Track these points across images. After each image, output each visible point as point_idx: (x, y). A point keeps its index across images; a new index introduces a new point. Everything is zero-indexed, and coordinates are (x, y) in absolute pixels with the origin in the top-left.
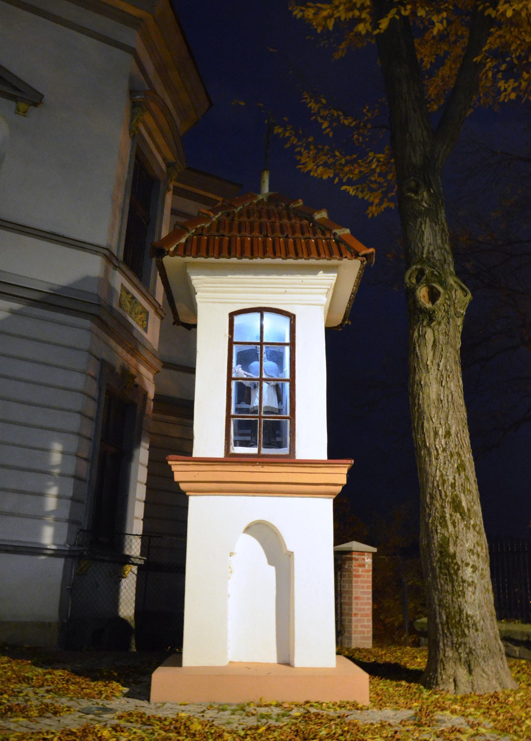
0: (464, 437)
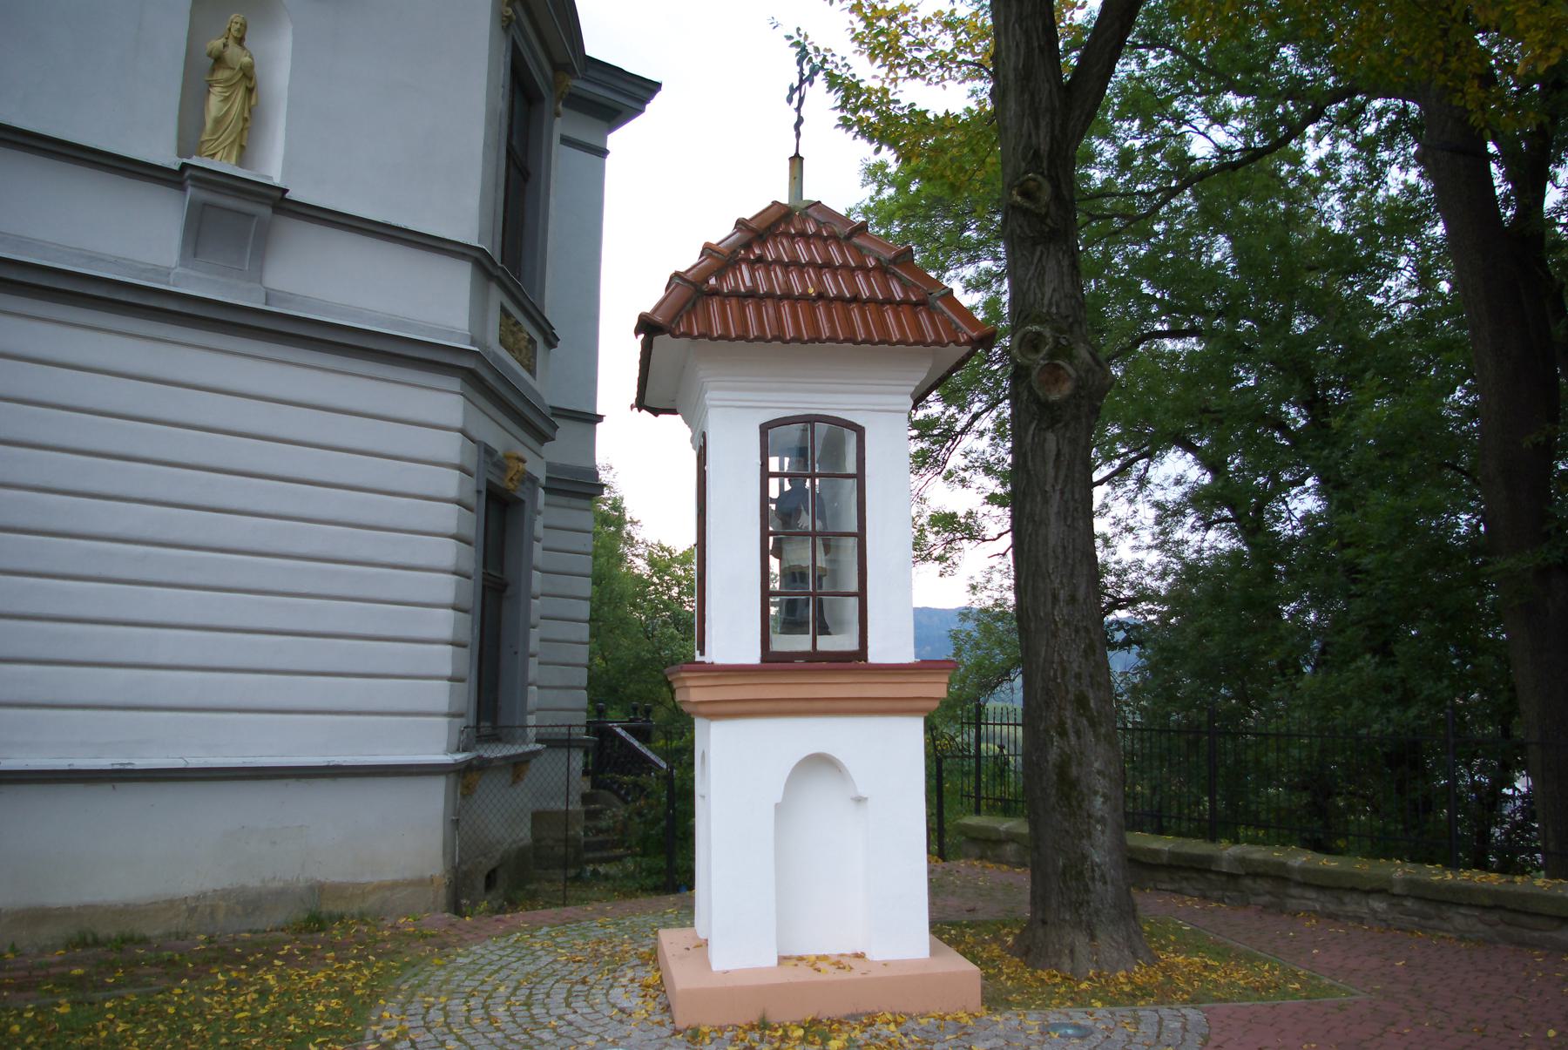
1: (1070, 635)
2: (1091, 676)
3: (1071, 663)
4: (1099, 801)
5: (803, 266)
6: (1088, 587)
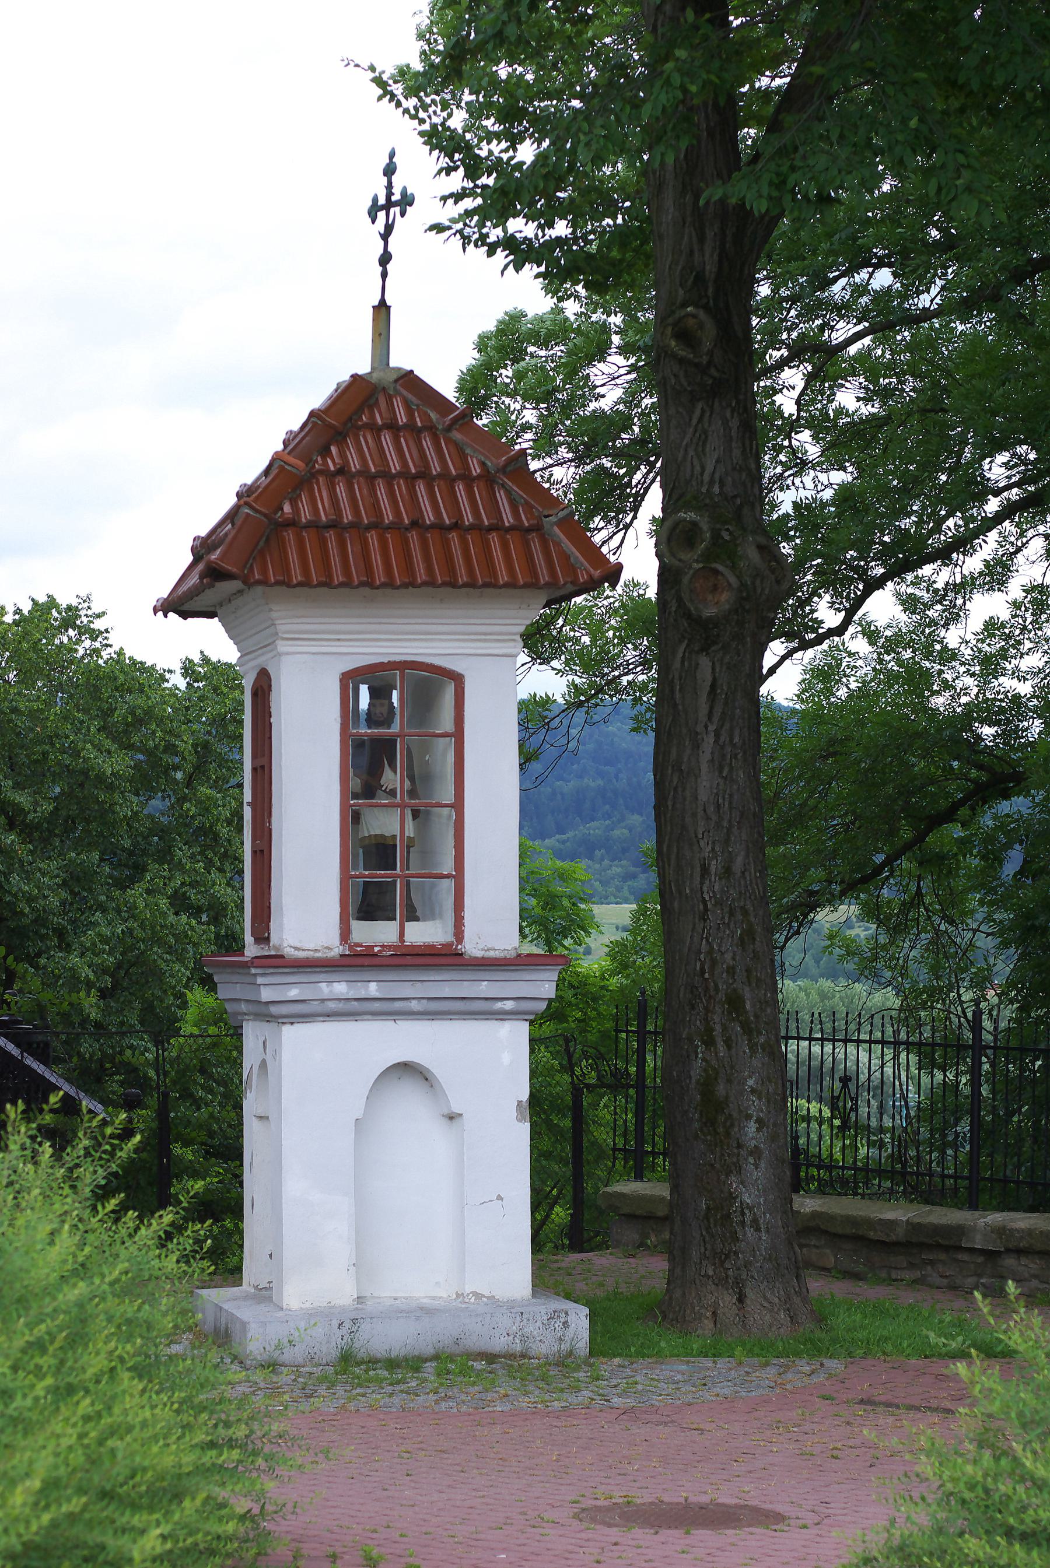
0: (756, 877)
1: (723, 918)
2: (748, 971)
3: (723, 954)
4: (752, 1127)
5: (394, 477)
6: (747, 856)
